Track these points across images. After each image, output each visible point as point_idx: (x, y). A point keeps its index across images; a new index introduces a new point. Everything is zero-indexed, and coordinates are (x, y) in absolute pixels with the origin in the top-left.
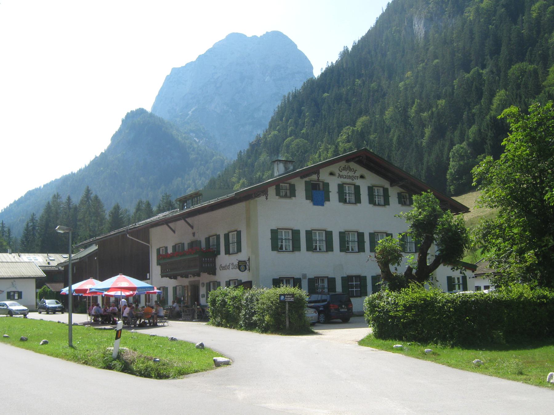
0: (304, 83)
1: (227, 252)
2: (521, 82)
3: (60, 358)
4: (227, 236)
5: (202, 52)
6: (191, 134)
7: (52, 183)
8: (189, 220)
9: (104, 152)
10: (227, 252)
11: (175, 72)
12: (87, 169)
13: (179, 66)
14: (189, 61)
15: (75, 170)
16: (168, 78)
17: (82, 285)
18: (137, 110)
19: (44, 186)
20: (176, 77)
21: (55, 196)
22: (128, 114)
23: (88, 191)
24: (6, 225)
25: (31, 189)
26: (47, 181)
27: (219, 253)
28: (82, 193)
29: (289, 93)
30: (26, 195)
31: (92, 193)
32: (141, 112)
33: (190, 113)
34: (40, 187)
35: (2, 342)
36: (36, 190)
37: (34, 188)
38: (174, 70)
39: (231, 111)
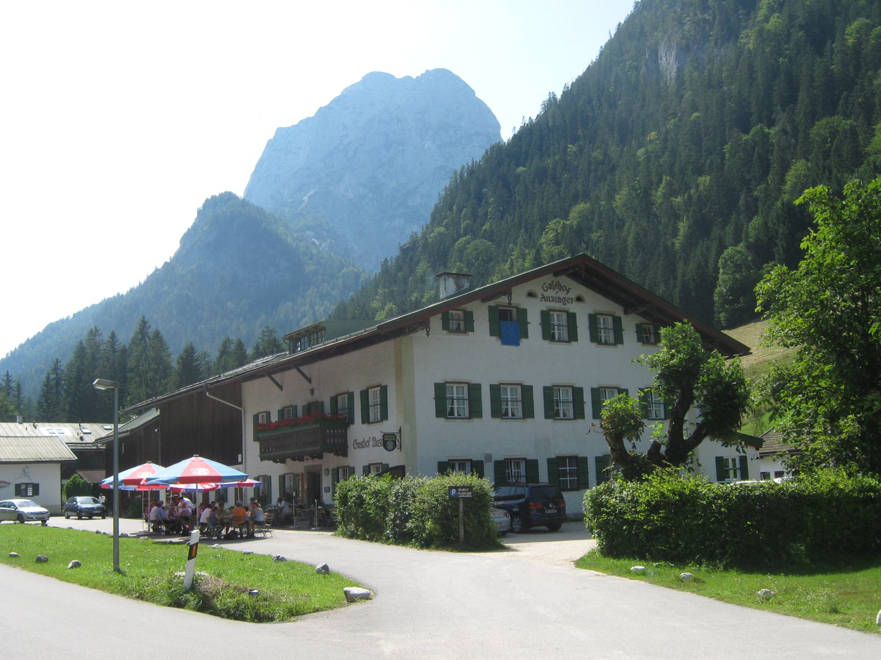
1: (366, 420)
4: (365, 395)
10: (366, 420)
15: (124, 291)
17: (132, 474)
21: (91, 331)
23: (144, 324)
24: (14, 378)
27: (351, 421)
28: (135, 327)
29: (463, 167)
31: (150, 327)
32: (228, 197)
33: (305, 198)
39: (370, 195)
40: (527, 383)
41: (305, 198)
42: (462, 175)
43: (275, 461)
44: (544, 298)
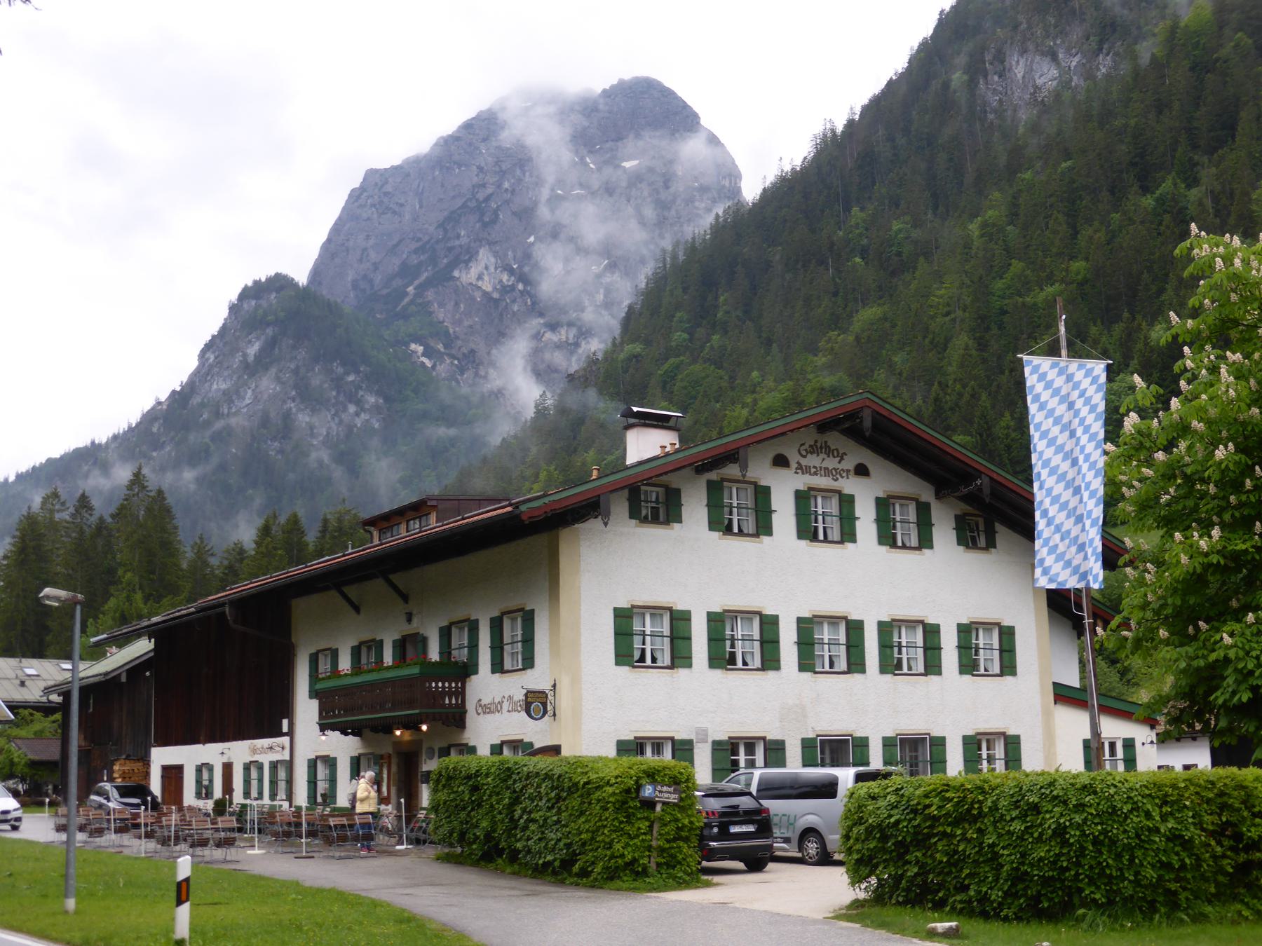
6: (413, 346)
8: (351, 591)
40: (768, 611)
41: (410, 289)
42: (674, 257)
43: (345, 733)
44: (802, 469)
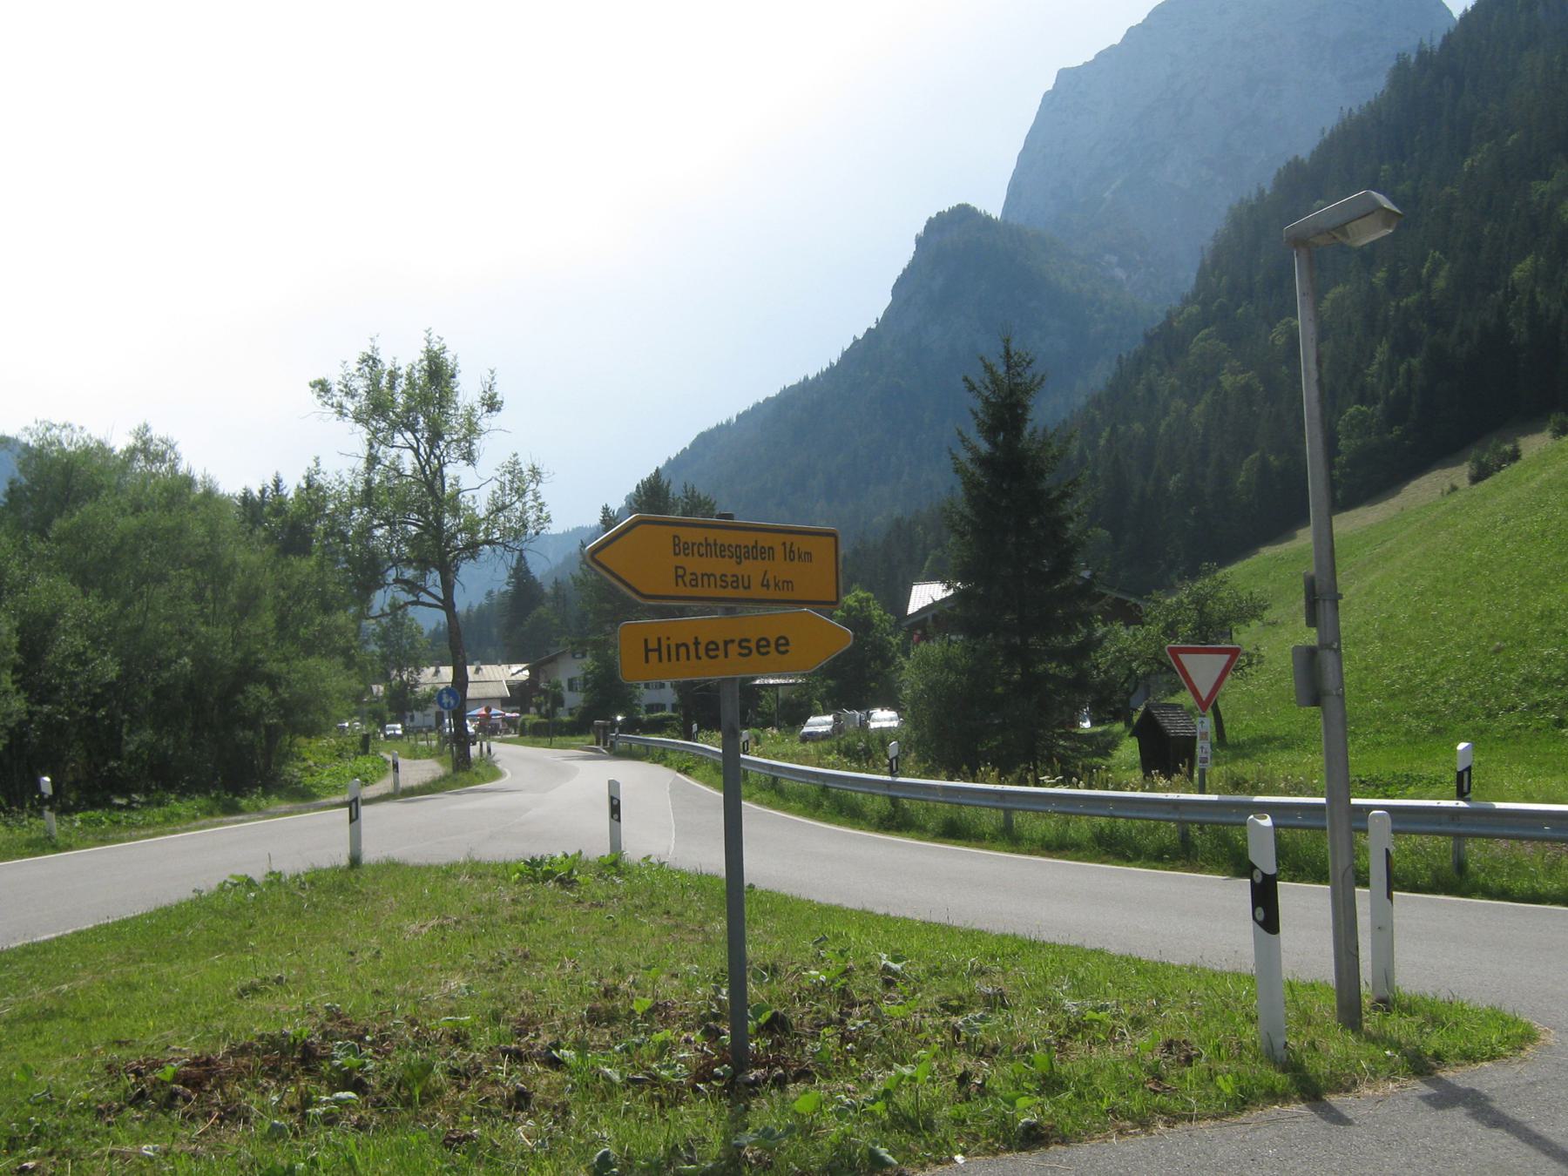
0: (1279, 173)
2: (291, 965)
3: (429, 868)
5: (1138, 17)
7: (757, 408)
9: (874, 326)
11: (1068, 78)
12: (892, 314)
13: (1076, 61)
14: (1104, 46)
16: (1049, 100)
18: (953, 211)
19: (738, 417)
20: (1069, 96)
22: (930, 221)
25: (704, 429)
26: (745, 404)
30: (693, 445)
32: (963, 214)
34: (729, 422)
35: (1432, 104)
36: (719, 428)
37: (713, 425)
38: (1063, 74)
